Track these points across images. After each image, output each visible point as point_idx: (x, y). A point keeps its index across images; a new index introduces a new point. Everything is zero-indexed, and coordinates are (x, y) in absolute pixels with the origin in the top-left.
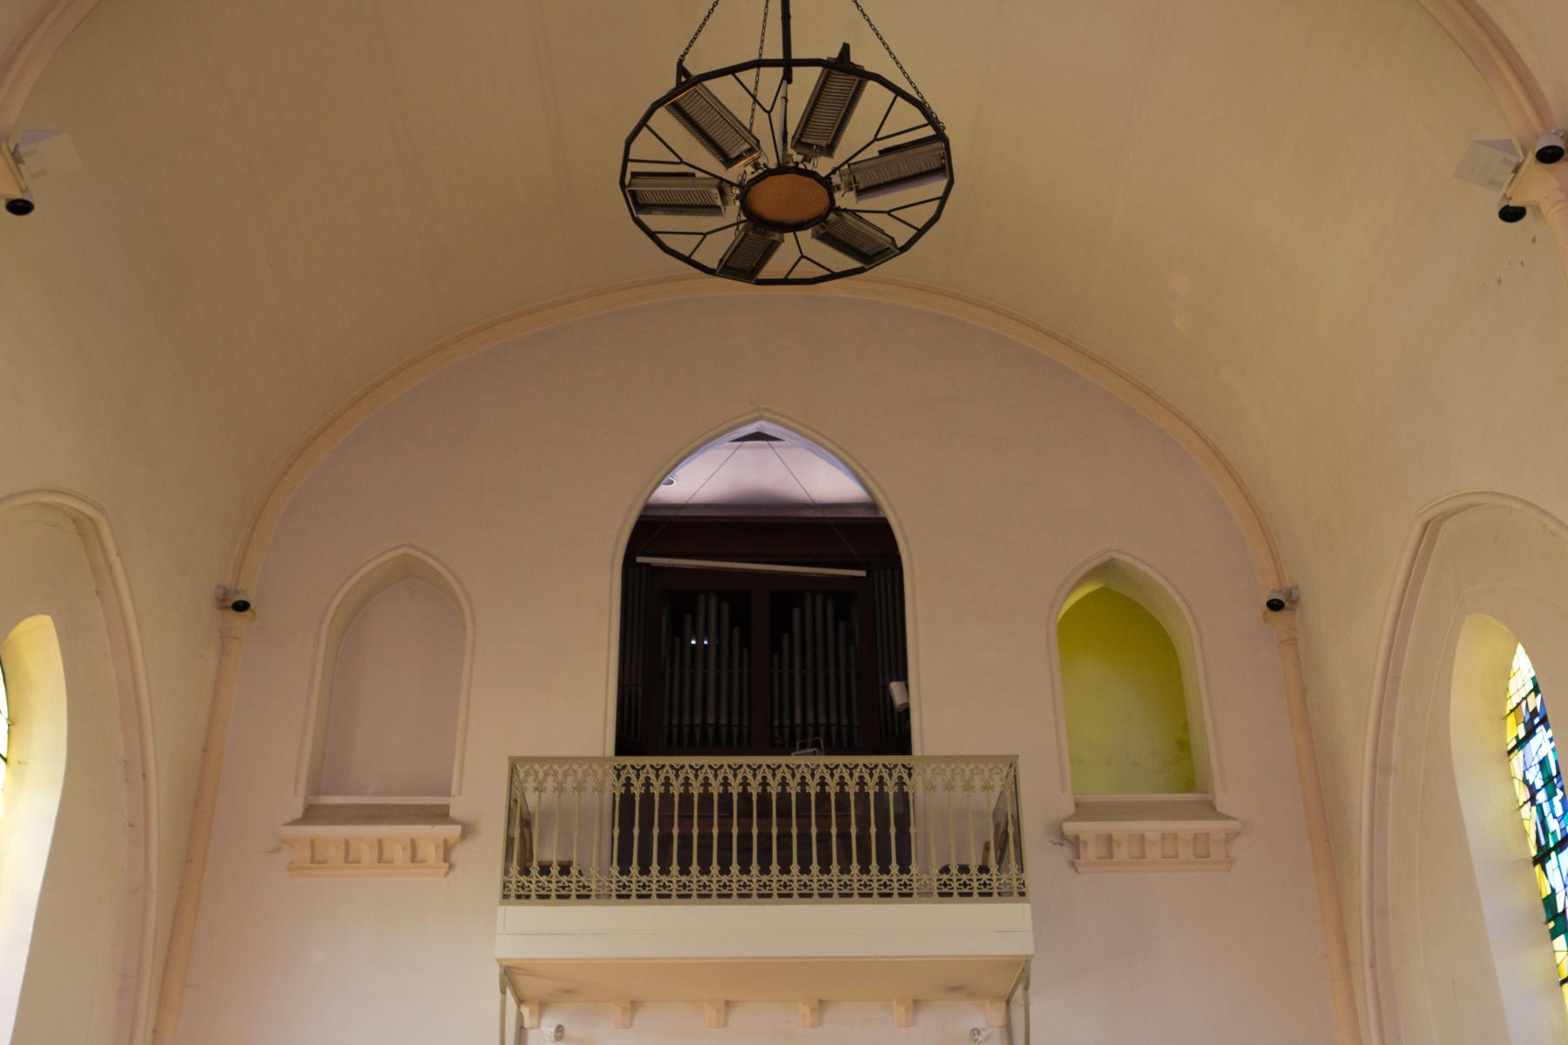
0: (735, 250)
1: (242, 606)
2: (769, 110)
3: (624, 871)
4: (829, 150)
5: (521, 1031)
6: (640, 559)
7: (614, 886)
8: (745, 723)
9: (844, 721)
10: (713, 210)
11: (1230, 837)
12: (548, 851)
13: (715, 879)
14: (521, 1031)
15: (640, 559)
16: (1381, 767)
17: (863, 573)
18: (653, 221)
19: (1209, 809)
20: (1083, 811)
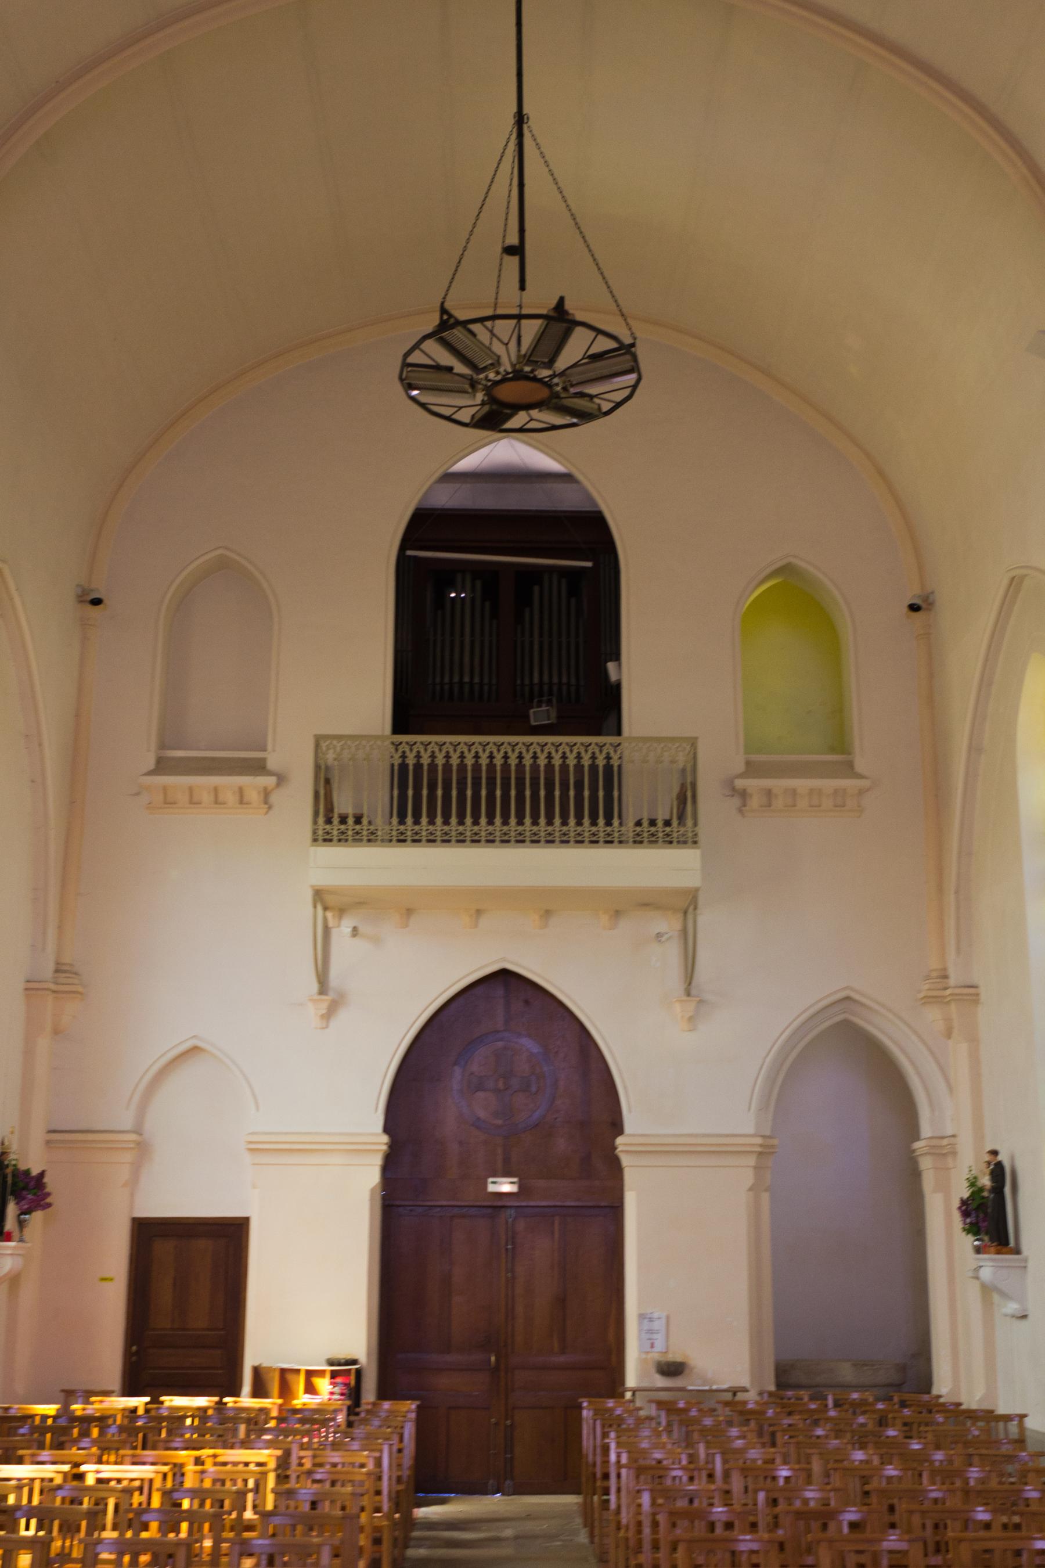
1: (97, 602)
2: (504, 346)
3: (402, 821)
5: (327, 930)
6: (409, 553)
7: (394, 833)
8: (494, 681)
9: (573, 681)
11: (861, 792)
12: (344, 804)
13: (469, 829)
14: (327, 930)
15: (409, 553)
16: (975, 749)
17: (589, 564)
19: (848, 769)
20: (752, 769)
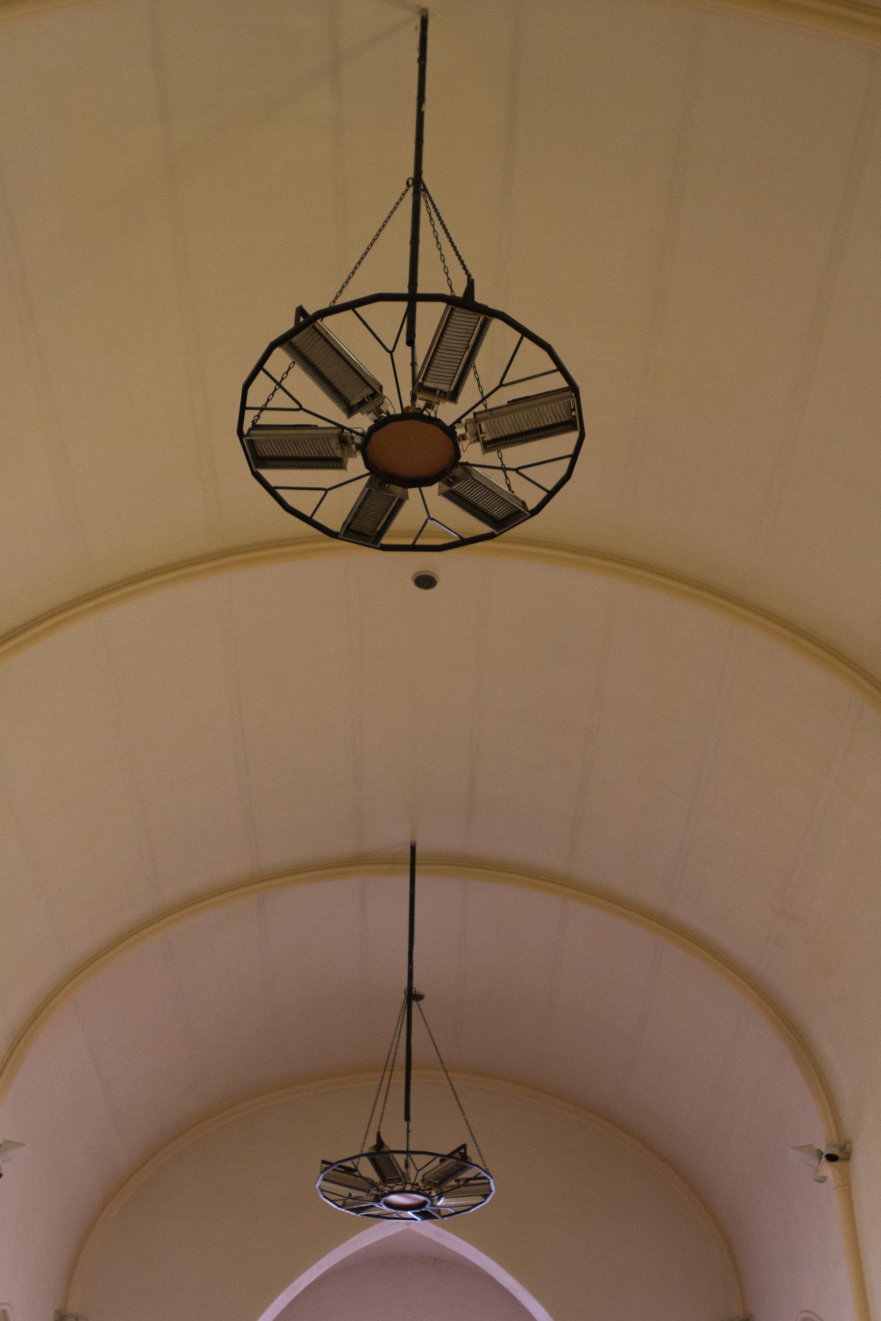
0: (358, 511)
4: (453, 396)
10: (337, 463)
18: (273, 476)
